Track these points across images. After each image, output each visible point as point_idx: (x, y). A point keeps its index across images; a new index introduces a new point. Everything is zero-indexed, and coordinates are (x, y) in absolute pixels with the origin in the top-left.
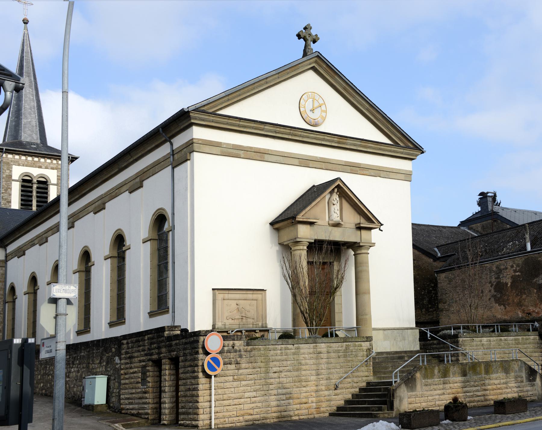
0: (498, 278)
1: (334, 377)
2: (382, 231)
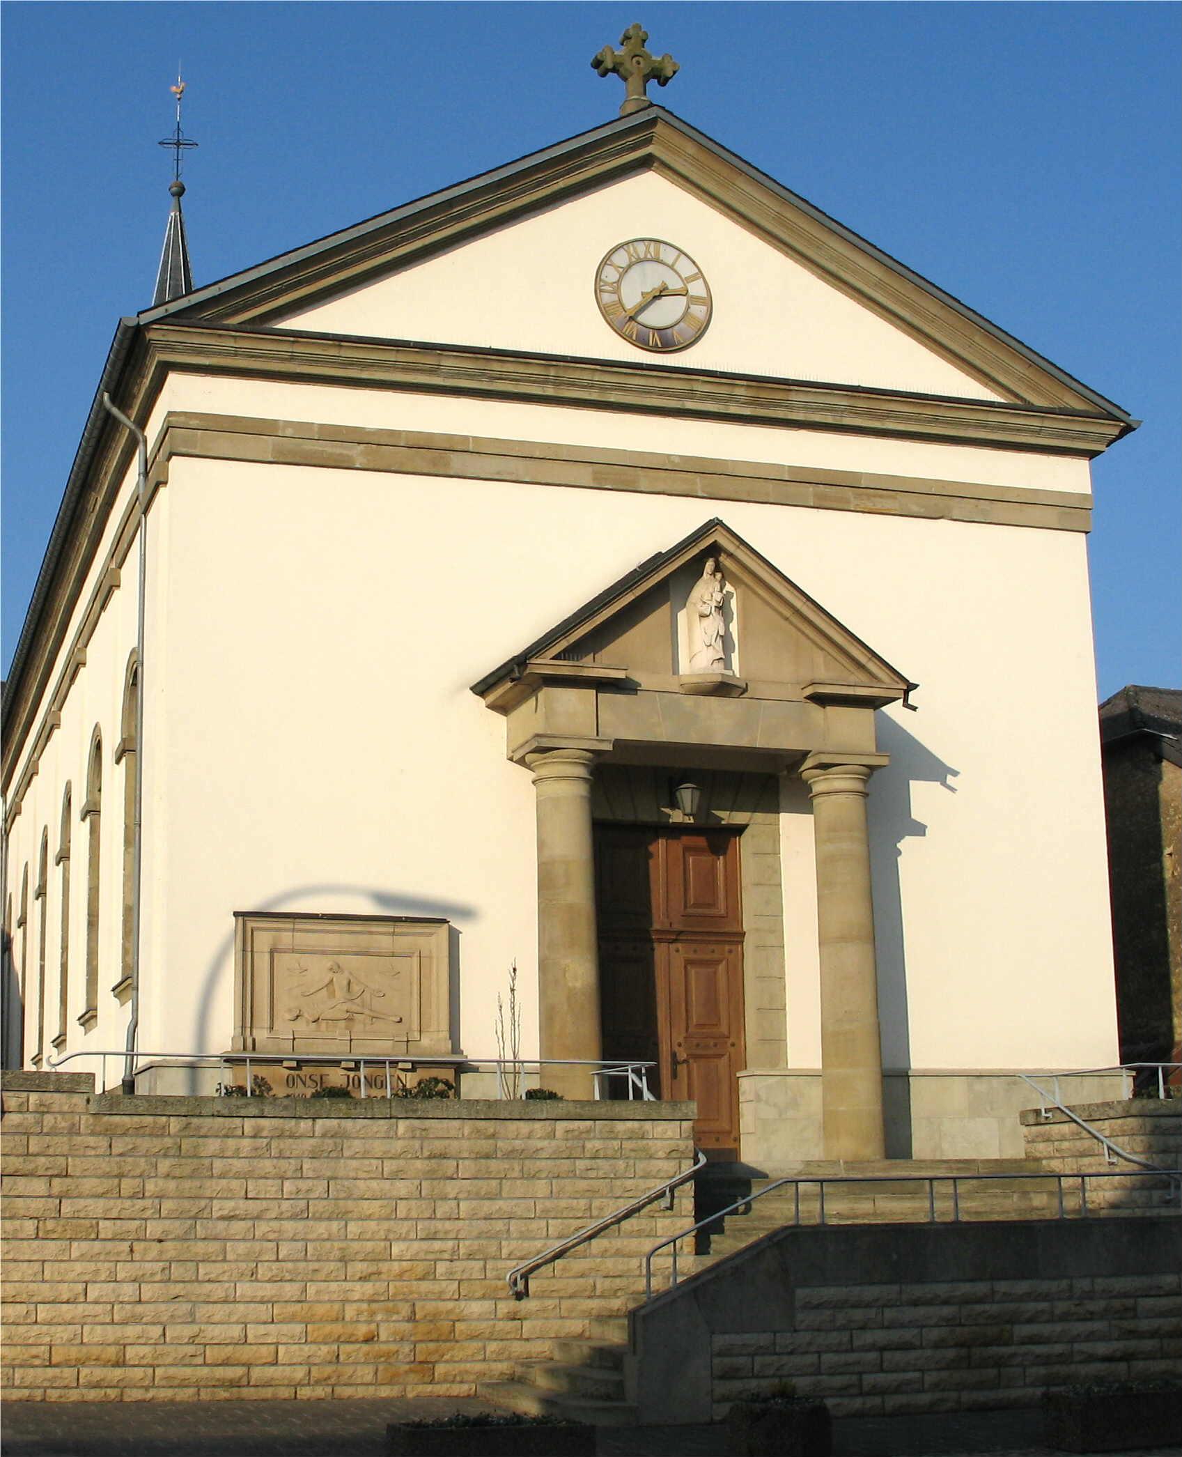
2: (914, 709)
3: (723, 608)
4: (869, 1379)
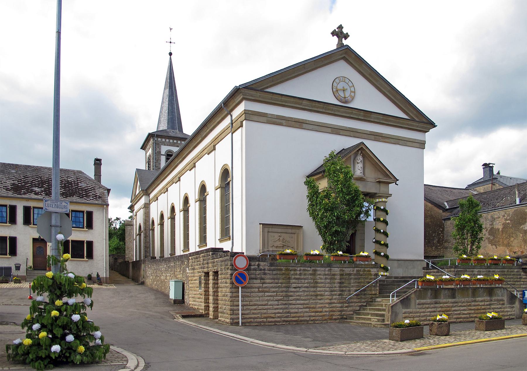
0: (492, 224)
1: (345, 294)
2: (398, 185)
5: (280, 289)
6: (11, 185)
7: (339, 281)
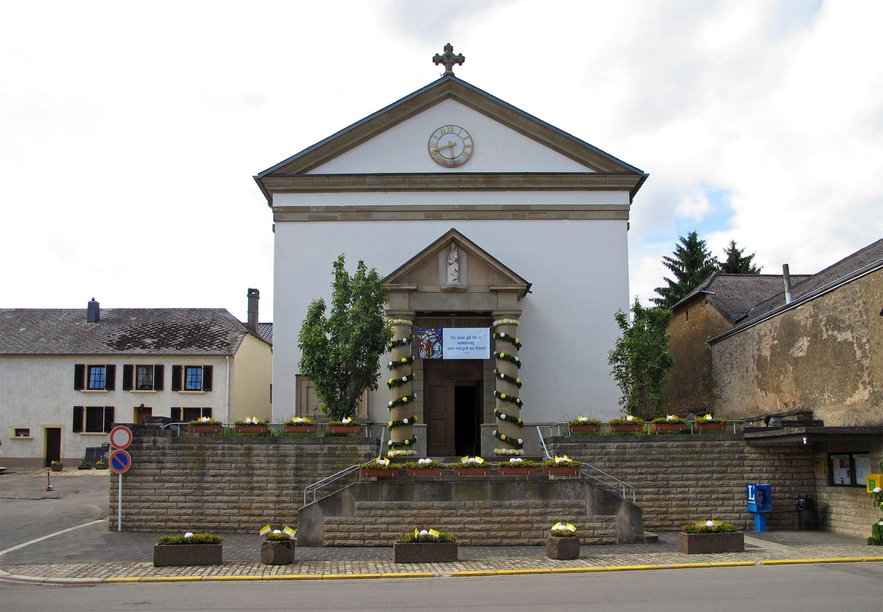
0: (759, 350)
3: (458, 261)
4: (382, 534)
5: (189, 478)
6: (119, 338)
7: (293, 465)
